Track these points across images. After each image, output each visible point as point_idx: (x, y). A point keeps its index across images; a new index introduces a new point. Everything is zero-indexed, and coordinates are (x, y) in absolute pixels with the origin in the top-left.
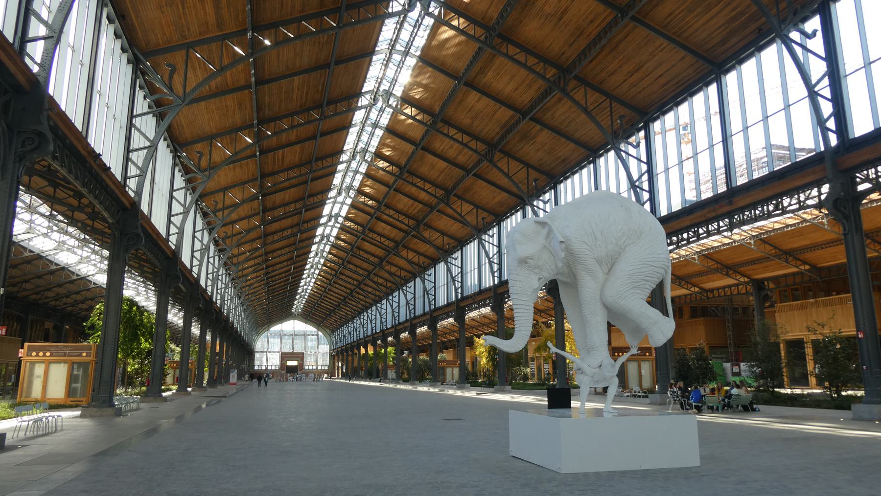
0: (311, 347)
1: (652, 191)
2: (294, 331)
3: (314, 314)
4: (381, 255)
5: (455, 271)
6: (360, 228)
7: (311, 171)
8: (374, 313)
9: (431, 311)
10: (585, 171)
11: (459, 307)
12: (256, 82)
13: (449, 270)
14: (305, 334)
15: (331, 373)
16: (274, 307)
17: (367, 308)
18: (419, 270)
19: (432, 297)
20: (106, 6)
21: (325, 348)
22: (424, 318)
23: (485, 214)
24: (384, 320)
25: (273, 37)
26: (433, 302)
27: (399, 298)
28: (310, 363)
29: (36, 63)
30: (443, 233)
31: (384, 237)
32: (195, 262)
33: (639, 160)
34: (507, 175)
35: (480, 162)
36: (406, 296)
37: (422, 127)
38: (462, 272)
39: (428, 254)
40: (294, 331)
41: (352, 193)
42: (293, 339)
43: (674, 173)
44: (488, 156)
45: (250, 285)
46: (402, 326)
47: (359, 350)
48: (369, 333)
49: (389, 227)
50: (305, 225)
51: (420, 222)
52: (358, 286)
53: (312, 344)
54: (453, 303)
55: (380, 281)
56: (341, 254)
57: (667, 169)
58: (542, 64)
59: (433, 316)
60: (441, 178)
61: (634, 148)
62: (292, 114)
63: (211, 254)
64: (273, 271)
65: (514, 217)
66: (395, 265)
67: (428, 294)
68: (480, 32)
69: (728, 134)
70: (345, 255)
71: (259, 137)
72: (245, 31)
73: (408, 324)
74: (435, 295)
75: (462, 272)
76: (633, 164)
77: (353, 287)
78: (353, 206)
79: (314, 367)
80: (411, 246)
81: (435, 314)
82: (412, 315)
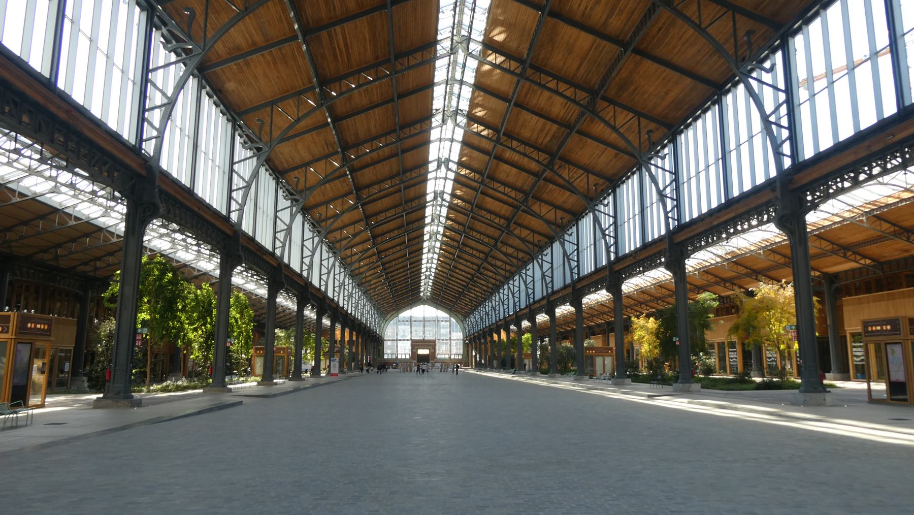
0: (443, 335)
1: (793, 127)
2: (424, 318)
3: (443, 297)
4: (507, 214)
5: (606, 221)
6: (477, 176)
7: (402, 182)
8: (506, 292)
9: (574, 283)
10: (709, 115)
11: (612, 274)
12: (333, 121)
13: (596, 220)
14: (437, 321)
15: (466, 362)
16: (399, 293)
17: (497, 288)
18: (557, 231)
19: (574, 264)
20: (205, 88)
21: (458, 335)
22: (565, 292)
23: (652, 126)
24: (530, 291)
25: (338, 88)
26: (576, 270)
27: (534, 271)
28: (442, 352)
29: (154, 127)
30: (588, 170)
31: (509, 187)
32: (336, 294)
33: (775, 88)
34: (614, 128)
35: (544, 171)
36: (541, 267)
37: (508, 76)
38: (615, 223)
39: (567, 206)
40: (424, 318)
41: (462, 120)
42: (424, 326)
43: (745, 149)
44: (590, 109)
45: (375, 288)
46: (537, 305)
47: (492, 337)
48: (502, 318)
49: (514, 170)
50: (408, 174)
51: (555, 156)
52: (485, 260)
53: (444, 331)
54: (603, 268)
55: (510, 250)
56: (461, 218)
57: (739, 146)
58: (572, 89)
59: (575, 291)
60: (582, 71)
61: (769, 78)
62: (372, 139)
63: (337, 271)
64: (390, 267)
65: (630, 181)
66: (526, 228)
67: (569, 259)
68: (514, 65)
69: (898, 33)
70: (466, 216)
71: (345, 160)
72: (313, 88)
73: (544, 302)
74: (578, 261)
75: (615, 223)
76: (768, 93)
77: (479, 262)
78: (465, 143)
79: (447, 356)
80: (545, 196)
81: (579, 286)
82: (550, 290)
